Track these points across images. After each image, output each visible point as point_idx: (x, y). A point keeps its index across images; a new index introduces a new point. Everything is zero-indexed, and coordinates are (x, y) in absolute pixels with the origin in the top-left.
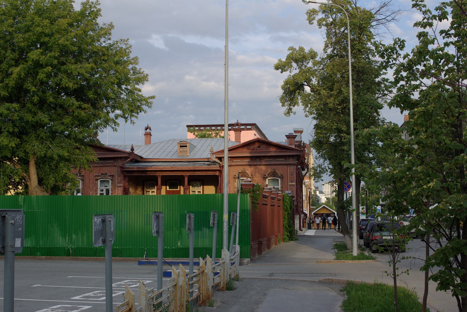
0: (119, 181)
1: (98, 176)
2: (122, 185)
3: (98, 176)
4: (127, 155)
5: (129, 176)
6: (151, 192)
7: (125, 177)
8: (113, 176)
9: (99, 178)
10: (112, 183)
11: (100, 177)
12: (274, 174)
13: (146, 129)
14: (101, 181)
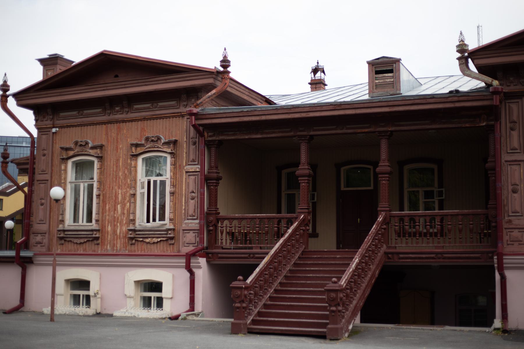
0: (191, 157)
1: (137, 146)
2: (197, 168)
4: (211, 81)
5: (221, 142)
6: (142, 191)
7: (209, 144)
8: (175, 142)
9: (140, 150)
10: (174, 164)
13: (315, 71)
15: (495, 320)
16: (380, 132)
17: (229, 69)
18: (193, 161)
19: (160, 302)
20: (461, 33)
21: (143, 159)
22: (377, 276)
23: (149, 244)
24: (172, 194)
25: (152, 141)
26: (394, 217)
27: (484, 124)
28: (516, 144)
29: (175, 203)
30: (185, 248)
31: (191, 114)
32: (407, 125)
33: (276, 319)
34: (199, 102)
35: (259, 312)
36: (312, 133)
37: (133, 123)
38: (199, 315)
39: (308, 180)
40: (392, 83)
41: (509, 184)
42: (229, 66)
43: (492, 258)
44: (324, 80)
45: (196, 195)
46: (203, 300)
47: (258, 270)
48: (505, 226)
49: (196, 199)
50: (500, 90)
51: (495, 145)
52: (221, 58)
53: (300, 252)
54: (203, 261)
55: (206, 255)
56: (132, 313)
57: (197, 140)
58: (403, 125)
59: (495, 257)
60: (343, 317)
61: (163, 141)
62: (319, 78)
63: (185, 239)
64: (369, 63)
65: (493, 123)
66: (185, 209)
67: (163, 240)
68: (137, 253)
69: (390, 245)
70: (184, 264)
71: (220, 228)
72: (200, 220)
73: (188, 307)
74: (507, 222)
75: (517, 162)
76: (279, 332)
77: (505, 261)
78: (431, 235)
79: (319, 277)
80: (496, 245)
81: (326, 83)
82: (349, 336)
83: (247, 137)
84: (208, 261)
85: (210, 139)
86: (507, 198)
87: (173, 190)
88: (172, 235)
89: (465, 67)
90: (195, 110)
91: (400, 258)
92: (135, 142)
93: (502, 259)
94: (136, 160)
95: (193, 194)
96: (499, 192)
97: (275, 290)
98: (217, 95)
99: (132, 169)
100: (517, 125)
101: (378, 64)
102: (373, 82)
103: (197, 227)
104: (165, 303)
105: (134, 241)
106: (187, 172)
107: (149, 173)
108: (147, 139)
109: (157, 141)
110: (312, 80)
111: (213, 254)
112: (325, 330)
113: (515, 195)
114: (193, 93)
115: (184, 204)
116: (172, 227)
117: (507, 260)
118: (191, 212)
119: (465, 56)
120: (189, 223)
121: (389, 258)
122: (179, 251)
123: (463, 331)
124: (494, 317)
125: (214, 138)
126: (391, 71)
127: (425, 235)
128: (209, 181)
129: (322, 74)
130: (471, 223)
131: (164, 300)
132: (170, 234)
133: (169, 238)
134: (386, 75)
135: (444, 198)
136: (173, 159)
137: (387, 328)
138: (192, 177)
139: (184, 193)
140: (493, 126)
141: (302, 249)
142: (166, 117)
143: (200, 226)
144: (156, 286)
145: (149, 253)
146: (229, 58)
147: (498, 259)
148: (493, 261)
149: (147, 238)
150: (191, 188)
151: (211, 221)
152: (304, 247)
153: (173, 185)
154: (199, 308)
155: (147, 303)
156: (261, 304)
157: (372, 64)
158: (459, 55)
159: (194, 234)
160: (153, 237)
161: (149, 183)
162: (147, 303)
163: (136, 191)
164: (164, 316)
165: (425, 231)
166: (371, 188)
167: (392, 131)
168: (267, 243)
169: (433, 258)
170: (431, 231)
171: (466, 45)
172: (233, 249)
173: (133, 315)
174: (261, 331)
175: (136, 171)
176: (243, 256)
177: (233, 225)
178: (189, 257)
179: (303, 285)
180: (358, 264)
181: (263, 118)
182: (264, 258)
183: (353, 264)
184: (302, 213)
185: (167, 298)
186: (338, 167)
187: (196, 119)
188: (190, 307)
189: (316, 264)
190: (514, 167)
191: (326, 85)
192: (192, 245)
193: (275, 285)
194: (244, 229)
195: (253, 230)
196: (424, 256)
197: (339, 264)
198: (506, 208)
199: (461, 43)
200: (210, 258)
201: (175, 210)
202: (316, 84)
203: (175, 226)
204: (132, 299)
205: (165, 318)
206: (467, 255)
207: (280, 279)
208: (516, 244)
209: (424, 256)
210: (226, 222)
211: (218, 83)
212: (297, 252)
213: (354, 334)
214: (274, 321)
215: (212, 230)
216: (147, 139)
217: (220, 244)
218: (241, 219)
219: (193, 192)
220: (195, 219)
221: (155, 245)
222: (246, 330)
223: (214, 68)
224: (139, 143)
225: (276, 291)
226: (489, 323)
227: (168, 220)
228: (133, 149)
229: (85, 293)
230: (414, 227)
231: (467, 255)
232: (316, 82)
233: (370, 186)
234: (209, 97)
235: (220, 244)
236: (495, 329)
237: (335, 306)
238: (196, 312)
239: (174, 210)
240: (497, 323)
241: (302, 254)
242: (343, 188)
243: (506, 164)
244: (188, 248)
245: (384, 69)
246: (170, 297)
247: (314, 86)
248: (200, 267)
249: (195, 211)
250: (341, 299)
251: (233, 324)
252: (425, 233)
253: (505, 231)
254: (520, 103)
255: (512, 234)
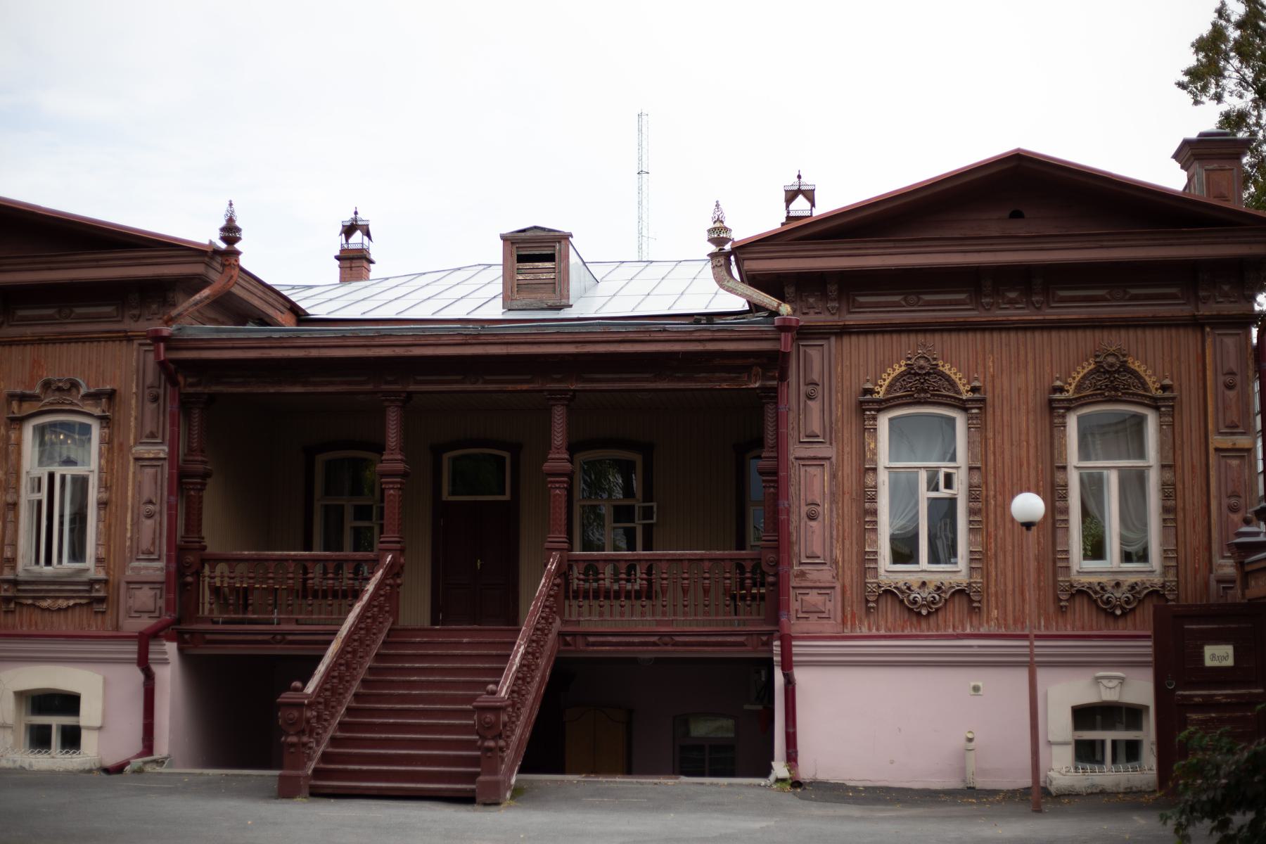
0: (147, 430)
1: (23, 398)
3: (23, 398)
4: (198, 269)
5: (212, 398)
6: (36, 496)
7: (186, 404)
8: (111, 395)
9: (28, 408)
10: (107, 442)
11: (36, 407)
12: (1112, 381)
13: (349, 230)
14: (41, 431)
15: (773, 764)
16: (551, 392)
17: (238, 246)
18: (152, 435)
19: (72, 739)
20: (717, 205)
21: (34, 427)
22: (547, 679)
23: (47, 614)
24: (103, 504)
25: (59, 389)
26: (576, 561)
27: (757, 385)
28: (816, 427)
29: (110, 525)
30: (131, 620)
31: (157, 338)
32: (607, 381)
33: (365, 768)
34: (174, 313)
35: (324, 754)
36: (412, 388)
37: (14, 348)
38: (163, 762)
39: (400, 483)
40: (553, 283)
41: (803, 502)
42: (237, 239)
43: (768, 644)
44: (367, 251)
45: (157, 508)
46: (171, 731)
47: (322, 668)
48: (794, 583)
49: (157, 517)
50: (794, 324)
51: (777, 425)
52: (223, 223)
53: (386, 631)
54: (171, 648)
55: (178, 637)
56: (14, 762)
57: (162, 391)
58: (599, 381)
59: (777, 643)
60: (502, 759)
61: (83, 391)
62: (359, 247)
63: (131, 602)
64: (504, 238)
65: (774, 383)
66: (131, 539)
67: (81, 605)
68: (19, 631)
69: (567, 617)
70: (136, 656)
71: (207, 579)
72: (169, 560)
73: (138, 746)
74: (796, 576)
75: (819, 461)
76: (375, 792)
77: (795, 650)
78: (628, 595)
79: (433, 682)
80: (777, 621)
81: (373, 257)
82: (512, 797)
83: (272, 390)
84: (180, 650)
85: (191, 390)
86: (798, 529)
87: (105, 496)
88: (102, 594)
89: (724, 273)
90: (167, 331)
91: (588, 644)
92: (18, 391)
93: (790, 646)
94: (20, 430)
95: (151, 507)
96: (783, 517)
97: (348, 709)
98: (212, 299)
99: (11, 448)
100: (819, 389)
101: (524, 241)
102: (512, 277)
103: (160, 576)
104: (87, 739)
105: (12, 605)
106: (137, 459)
107: (45, 459)
108: (47, 385)
109: (69, 390)
110: (342, 251)
111: (192, 633)
112: (473, 786)
113: (813, 524)
114: (157, 293)
115: (129, 527)
116: (102, 575)
117: (798, 648)
118: (146, 543)
119: (732, 255)
120: (140, 569)
121: (567, 644)
122: (117, 627)
123: (717, 784)
124: (771, 757)
125: (199, 389)
126: (550, 258)
127: (617, 595)
128: (185, 483)
129: (366, 238)
130: (728, 575)
131: (84, 734)
132: (97, 591)
133: (95, 599)
134: (540, 265)
135: (654, 521)
136: (106, 430)
137: (570, 782)
138: (150, 471)
139: (129, 503)
140: (775, 390)
141: (388, 625)
142: (91, 340)
143: (168, 574)
144: (69, 703)
145: (48, 631)
146: (238, 223)
147: (782, 646)
148: (772, 651)
149: (44, 598)
150: (148, 492)
151: (186, 563)
152: (391, 620)
153: (105, 485)
154: (163, 745)
155: (40, 738)
156: (327, 737)
157: (510, 240)
158: (713, 248)
159: (152, 593)
160: (58, 598)
161: (51, 476)
162: (40, 738)
163: (19, 496)
164: (87, 767)
165: (616, 587)
166: (507, 497)
167: (575, 391)
168: (292, 612)
169: (654, 644)
170: (629, 587)
171: (727, 230)
172: (224, 623)
173: (18, 765)
174: (336, 792)
175: (19, 454)
176: (260, 638)
177: (218, 572)
178: (145, 640)
179: (403, 698)
180: (524, 657)
181: (314, 353)
182: (329, 643)
183: (515, 656)
184: (389, 550)
185: (89, 728)
186: (437, 451)
187: (167, 349)
188: (145, 746)
189: (422, 655)
190: (812, 470)
191: (372, 262)
192: (146, 615)
193: (348, 700)
194: (242, 582)
195: (262, 583)
196: (636, 640)
197: (470, 656)
198: (796, 549)
199: (718, 225)
200: (186, 642)
201: (108, 541)
202: (351, 259)
203: (107, 573)
204: (9, 731)
205: (90, 771)
206: (720, 639)
207: (355, 687)
208: (813, 617)
209: (636, 640)
210: (221, 568)
211: (213, 275)
212: (380, 631)
213: (518, 793)
214: (361, 771)
215: (190, 584)
216: (47, 385)
217: (206, 612)
218: (254, 560)
219: (150, 502)
220: (154, 560)
221: (62, 614)
222: (307, 791)
223: (207, 242)
224: (28, 392)
225: (350, 711)
226: (765, 771)
227: (93, 559)
228: (15, 404)
229: (68, 720)
230: (597, 580)
231: (720, 639)
232: (351, 255)
233: (503, 493)
234: (196, 304)
235: (206, 612)
236: (778, 780)
237: (494, 738)
238: (156, 756)
239: (107, 537)
240: (780, 769)
241: (388, 635)
242: (446, 496)
243: (796, 464)
244: (139, 621)
245: (535, 251)
246: (98, 724)
247: (347, 264)
248: (165, 662)
249: (153, 543)
250: (308, 721)
251: (280, 776)
252: (615, 592)
253: (792, 593)
254: (826, 347)
255: (805, 598)
